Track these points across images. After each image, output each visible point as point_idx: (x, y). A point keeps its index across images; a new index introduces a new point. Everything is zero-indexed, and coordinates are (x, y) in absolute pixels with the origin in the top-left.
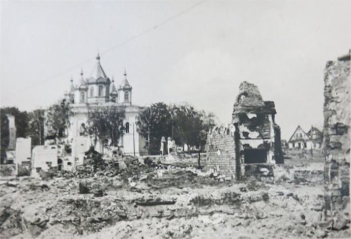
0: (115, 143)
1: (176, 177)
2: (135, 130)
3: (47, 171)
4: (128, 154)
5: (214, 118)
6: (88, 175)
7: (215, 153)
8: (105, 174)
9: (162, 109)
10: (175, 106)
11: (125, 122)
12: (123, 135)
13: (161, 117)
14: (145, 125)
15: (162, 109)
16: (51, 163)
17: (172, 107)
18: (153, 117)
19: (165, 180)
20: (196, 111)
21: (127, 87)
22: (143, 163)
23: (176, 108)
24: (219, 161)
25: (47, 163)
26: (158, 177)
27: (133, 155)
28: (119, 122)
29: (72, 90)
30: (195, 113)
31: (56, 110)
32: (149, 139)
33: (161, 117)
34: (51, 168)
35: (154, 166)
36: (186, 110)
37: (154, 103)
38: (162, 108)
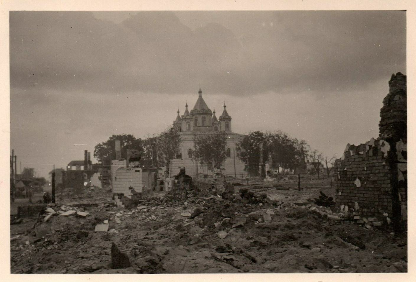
1: (295, 222)
2: (236, 155)
3: (130, 197)
4: (230, 175)
5: (304, 146)
6: (177, 202)
7: (351, 182)
8: (197, 201)
10: (270, 134)
11: (226, 148)
12: (225, 158)
19: (275, 228)
20: (289, 139)
21: (227, 117)
22: (240, 198)
23: (272, 136)
24: (358, 195)
26: (263, 221)
27: (234, 176)
29: (179, 121)
30: (288, 141)
31: (166, 137)
35: (256, 202)
36: (281, 138)
37: (252, 132)
38: (259, 136)
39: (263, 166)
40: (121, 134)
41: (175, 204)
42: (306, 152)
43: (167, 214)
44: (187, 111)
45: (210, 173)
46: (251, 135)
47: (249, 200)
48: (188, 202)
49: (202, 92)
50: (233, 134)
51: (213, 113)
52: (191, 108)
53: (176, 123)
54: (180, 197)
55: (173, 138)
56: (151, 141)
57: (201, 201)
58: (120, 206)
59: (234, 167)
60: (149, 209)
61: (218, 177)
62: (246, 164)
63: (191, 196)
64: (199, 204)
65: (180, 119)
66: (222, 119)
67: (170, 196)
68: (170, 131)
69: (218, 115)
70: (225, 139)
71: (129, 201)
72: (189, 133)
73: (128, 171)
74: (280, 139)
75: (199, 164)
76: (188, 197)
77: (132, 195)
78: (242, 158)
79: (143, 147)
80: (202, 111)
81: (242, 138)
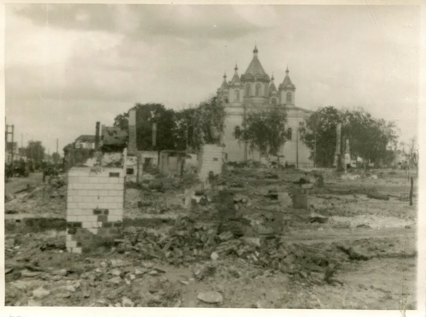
0: (274, 152)
3: (95, 232)
5: (392, 129)
8: (241, 251)
9: (332, 115)
10: (347, 112)
11: (286, 127)
13: (330, 123)
14: (311, 132)
15: (332, 115)
16: (107, 212)
17: (345, 113)
18: (321, 124)
20: (374, 119)
21: (289, 86)
23: (350, 114)
25: (97, 212)
28: (280, 128)
30: (372, 121)
32: (315, 149)
33: (330, 123)
34: (107, 225)
36: (362, 117)
38: (332, 113)
39: (341, 156)
40: (149, 103)
41: (189, 258)
42: (395, 137)
43: (163, 295)
44: (236, 76)
45: (264, 161)
46: (321, 110)
47: (303, 189)
48: (219, 253)
49: (259, 51)
50: (297, 109)
51: (271, 80)
52: (241, 72)
53: (221, 91)
54: (202, 239)
55: (215, 111)
56: (188, 114)
57: (250, 252)
58: (72, 249)
59: (295, 152)
60: (125, 273)
61: (274, 167)
62: (312, 151)
63: (228, 237)
64: (245, 258)
65: (227, 86)
66: (282, 88)
67: (181, 233)
68: (212, 102)
69: (277, 82)
70: (285, 115)
71: (91, 240)
72: (237, 104)
73: (93, 174)
74: (361, 118)
75: (248, 148)
76: (221, 241)
77: (99, 228)
78: (307, 141)
79: (176, 122)
80: (256, 76)
81: (309, 115)
